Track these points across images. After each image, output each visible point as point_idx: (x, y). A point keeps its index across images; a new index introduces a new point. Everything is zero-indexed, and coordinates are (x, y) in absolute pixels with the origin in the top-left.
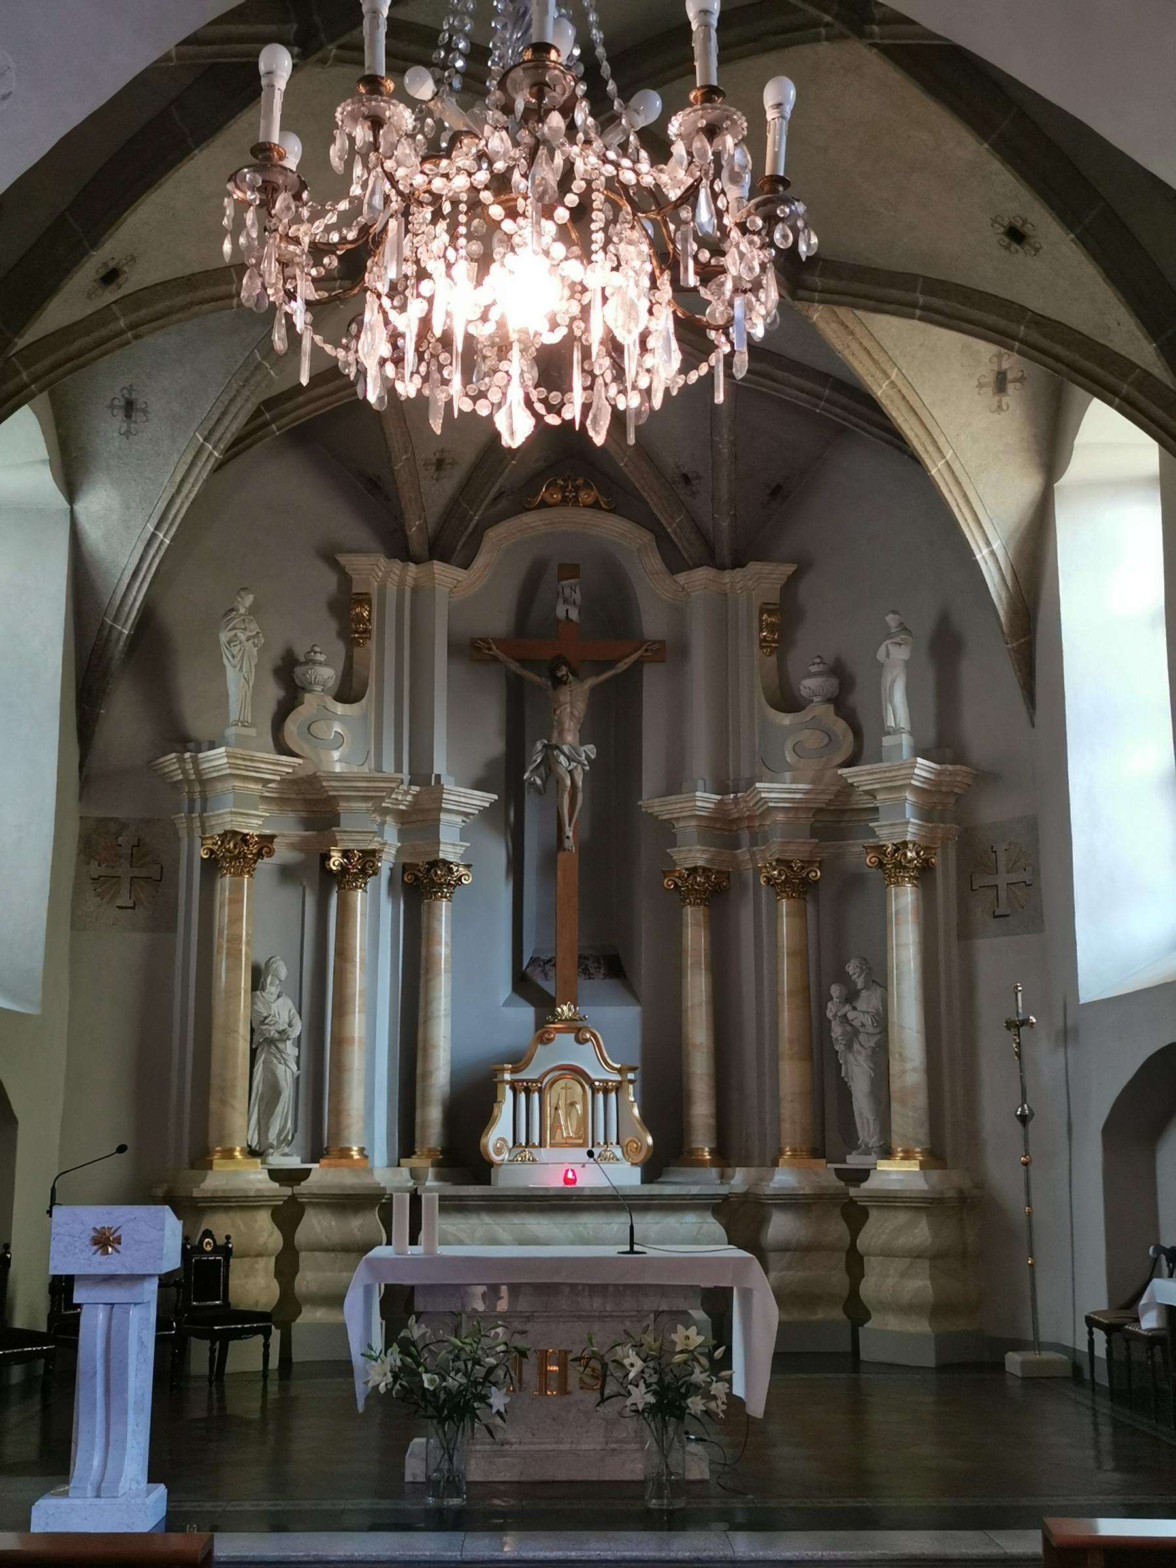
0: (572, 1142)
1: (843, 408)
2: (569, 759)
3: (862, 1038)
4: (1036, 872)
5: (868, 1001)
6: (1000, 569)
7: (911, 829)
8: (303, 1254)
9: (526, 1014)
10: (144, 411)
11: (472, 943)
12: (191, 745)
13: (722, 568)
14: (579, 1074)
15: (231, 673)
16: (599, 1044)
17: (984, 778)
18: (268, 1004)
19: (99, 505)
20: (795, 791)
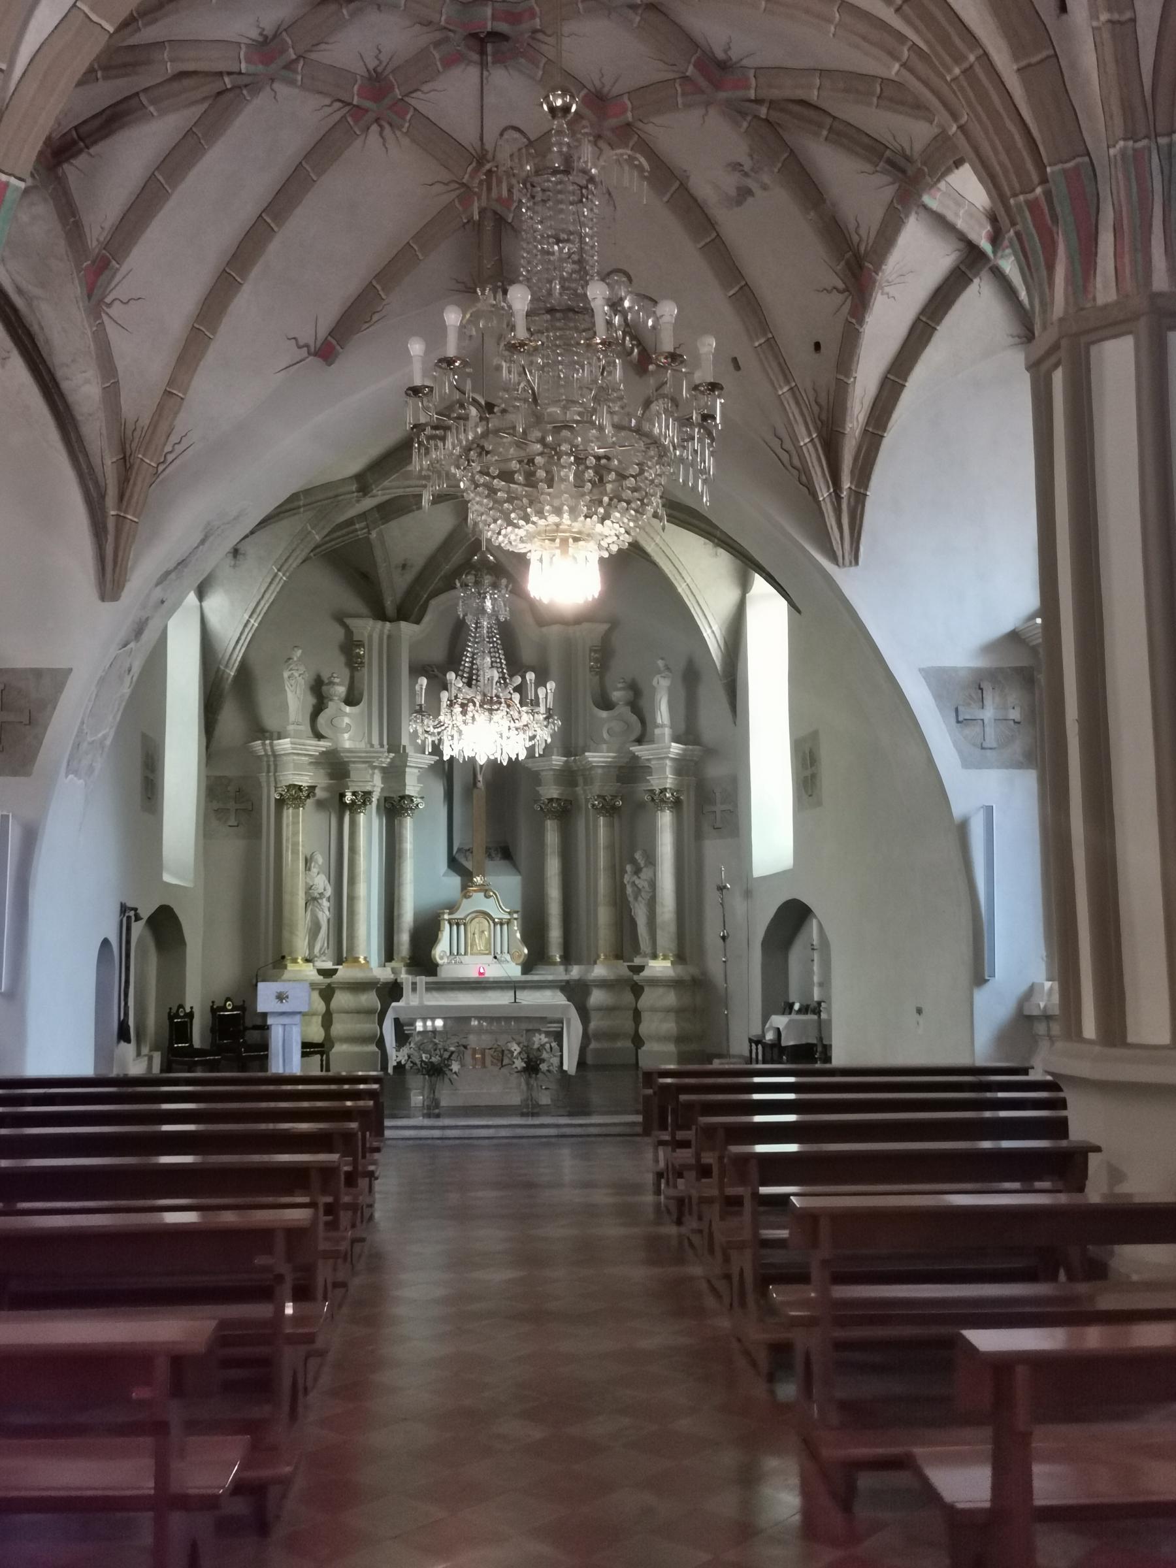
0: (483, 952)
3: (643, 894)
4: (736, 806)
5: (646, 874)
7: (669, 781)
8: (334, 1016)
9: (456, 881)
11: (424, 842)
12: (267, 735)
14: (486, 915)
15: (290, 695)
16: (497, 899)
17: (710, 752)
18: (312, 879)
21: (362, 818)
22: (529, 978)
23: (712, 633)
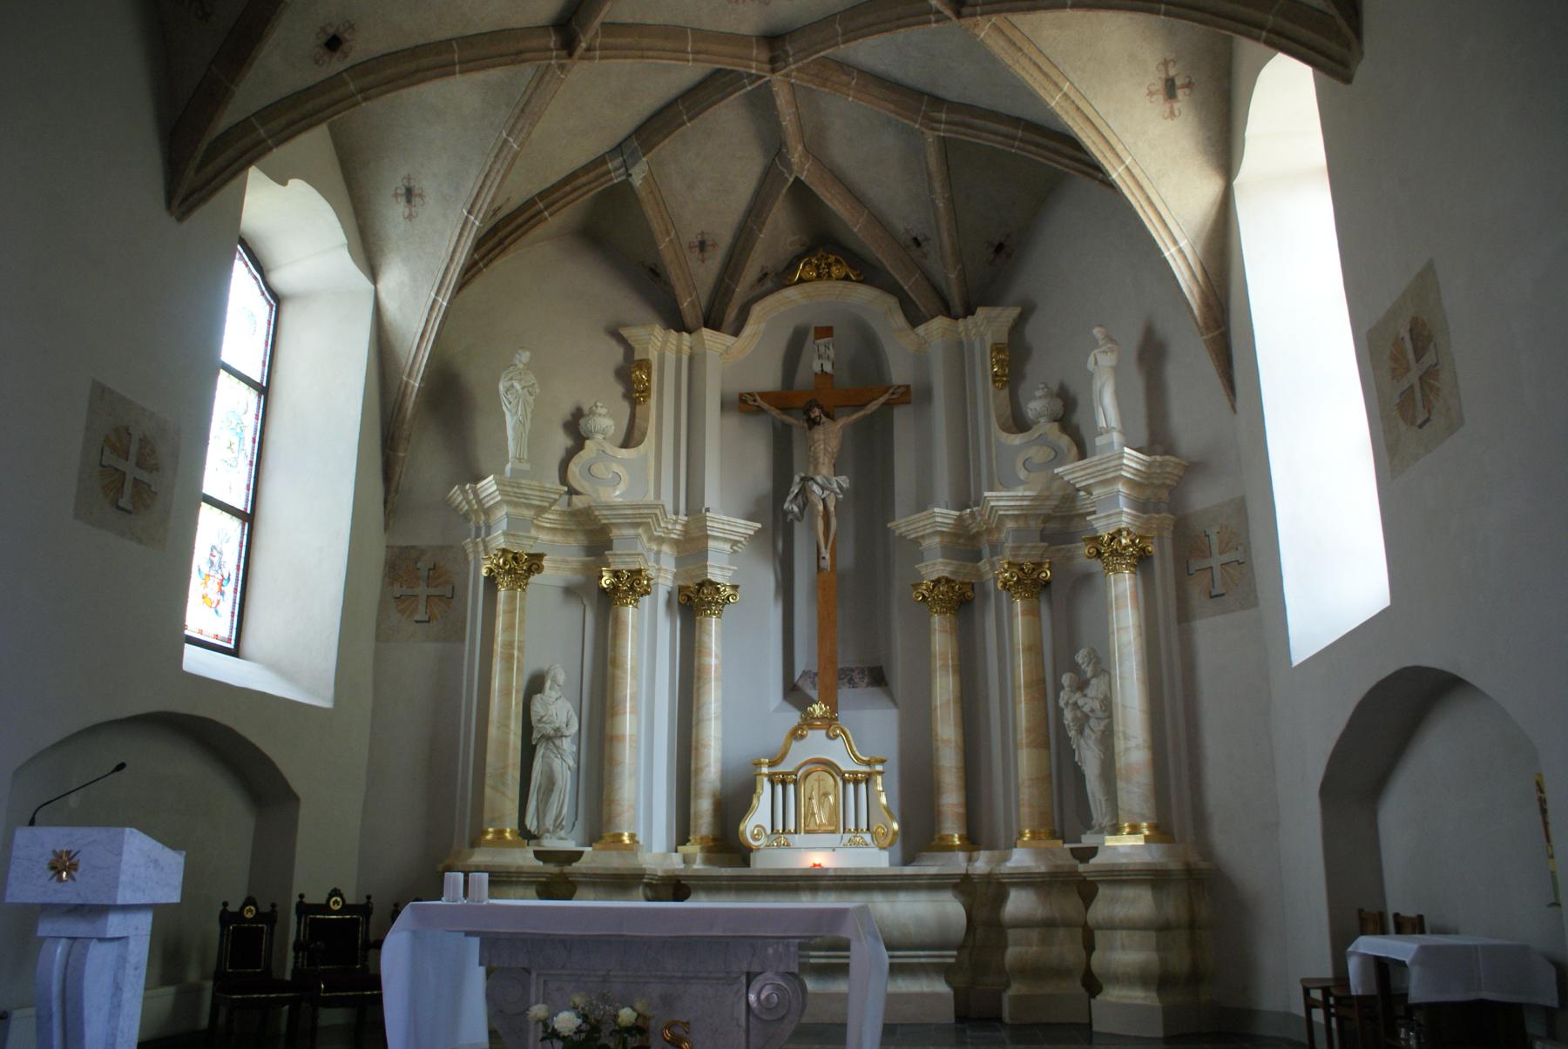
1: (1037, 145)
2: (823, 488)
3: (1092, 722)
4: (1247, 550)
5: (1096, 688)
6: (1189, 266)
9: (793, 717)
10: (421, 196)
11: (743, 658)
13: (956, 318)
14: (829, 766)
17: (1193, 468)
18: (546, 705)
19: (394, 278)
20: (1023, 498)
21: (629, 613)
22: (909, 870)
23: (1180, 251)
